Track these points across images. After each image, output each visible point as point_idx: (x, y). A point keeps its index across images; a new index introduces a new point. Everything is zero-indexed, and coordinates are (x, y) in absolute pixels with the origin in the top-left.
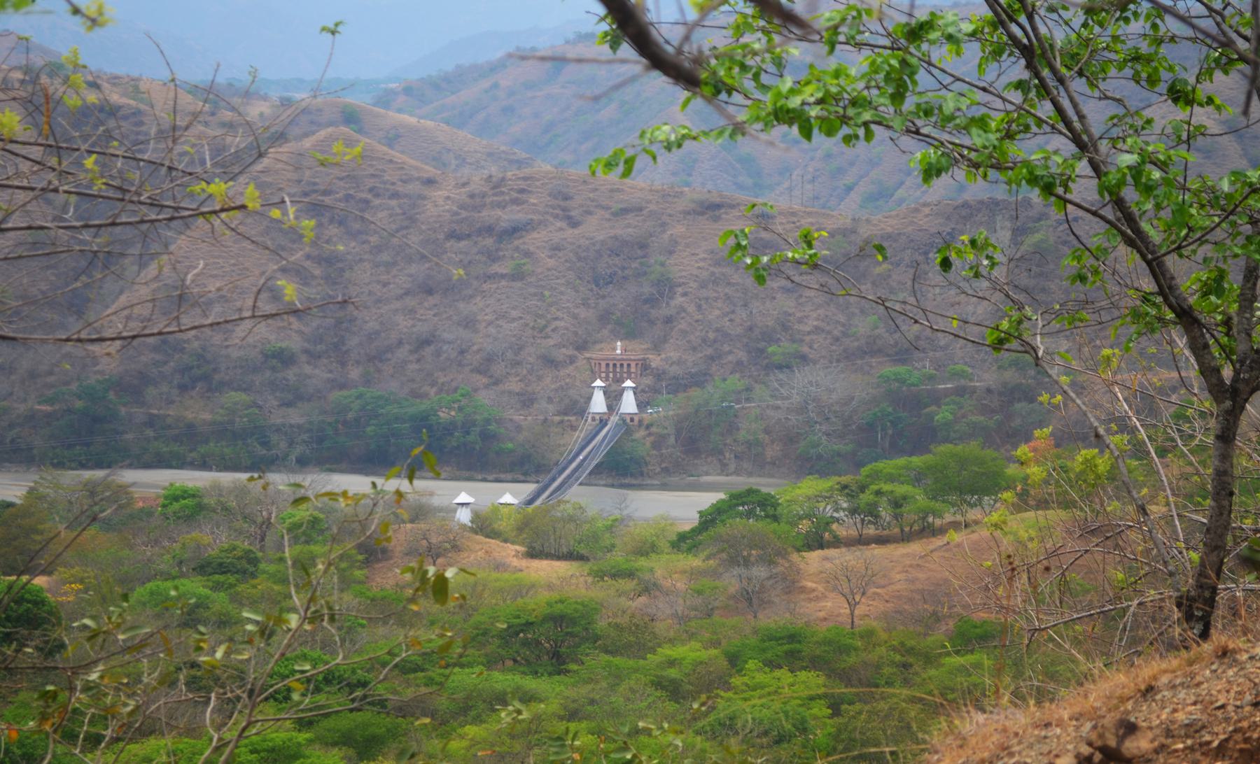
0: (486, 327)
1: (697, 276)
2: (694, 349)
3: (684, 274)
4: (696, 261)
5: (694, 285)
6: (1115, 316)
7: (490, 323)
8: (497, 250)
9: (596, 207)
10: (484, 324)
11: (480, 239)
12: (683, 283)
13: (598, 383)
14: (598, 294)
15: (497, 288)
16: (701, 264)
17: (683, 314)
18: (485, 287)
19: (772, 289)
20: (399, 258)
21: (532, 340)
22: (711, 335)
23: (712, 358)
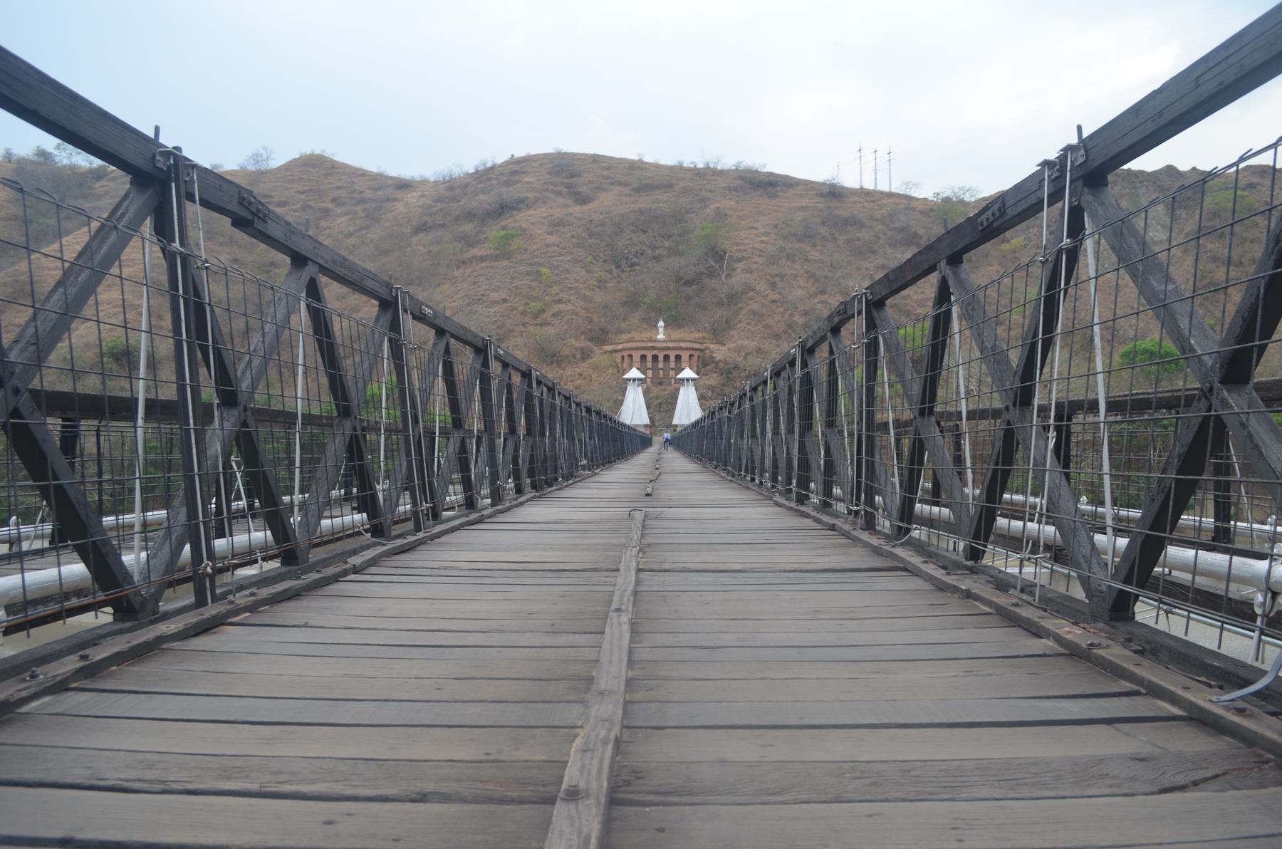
1: (761, 251)
2: (778, 337)
4: (757, 236)
5: (761, 260)
18: (457, 273)
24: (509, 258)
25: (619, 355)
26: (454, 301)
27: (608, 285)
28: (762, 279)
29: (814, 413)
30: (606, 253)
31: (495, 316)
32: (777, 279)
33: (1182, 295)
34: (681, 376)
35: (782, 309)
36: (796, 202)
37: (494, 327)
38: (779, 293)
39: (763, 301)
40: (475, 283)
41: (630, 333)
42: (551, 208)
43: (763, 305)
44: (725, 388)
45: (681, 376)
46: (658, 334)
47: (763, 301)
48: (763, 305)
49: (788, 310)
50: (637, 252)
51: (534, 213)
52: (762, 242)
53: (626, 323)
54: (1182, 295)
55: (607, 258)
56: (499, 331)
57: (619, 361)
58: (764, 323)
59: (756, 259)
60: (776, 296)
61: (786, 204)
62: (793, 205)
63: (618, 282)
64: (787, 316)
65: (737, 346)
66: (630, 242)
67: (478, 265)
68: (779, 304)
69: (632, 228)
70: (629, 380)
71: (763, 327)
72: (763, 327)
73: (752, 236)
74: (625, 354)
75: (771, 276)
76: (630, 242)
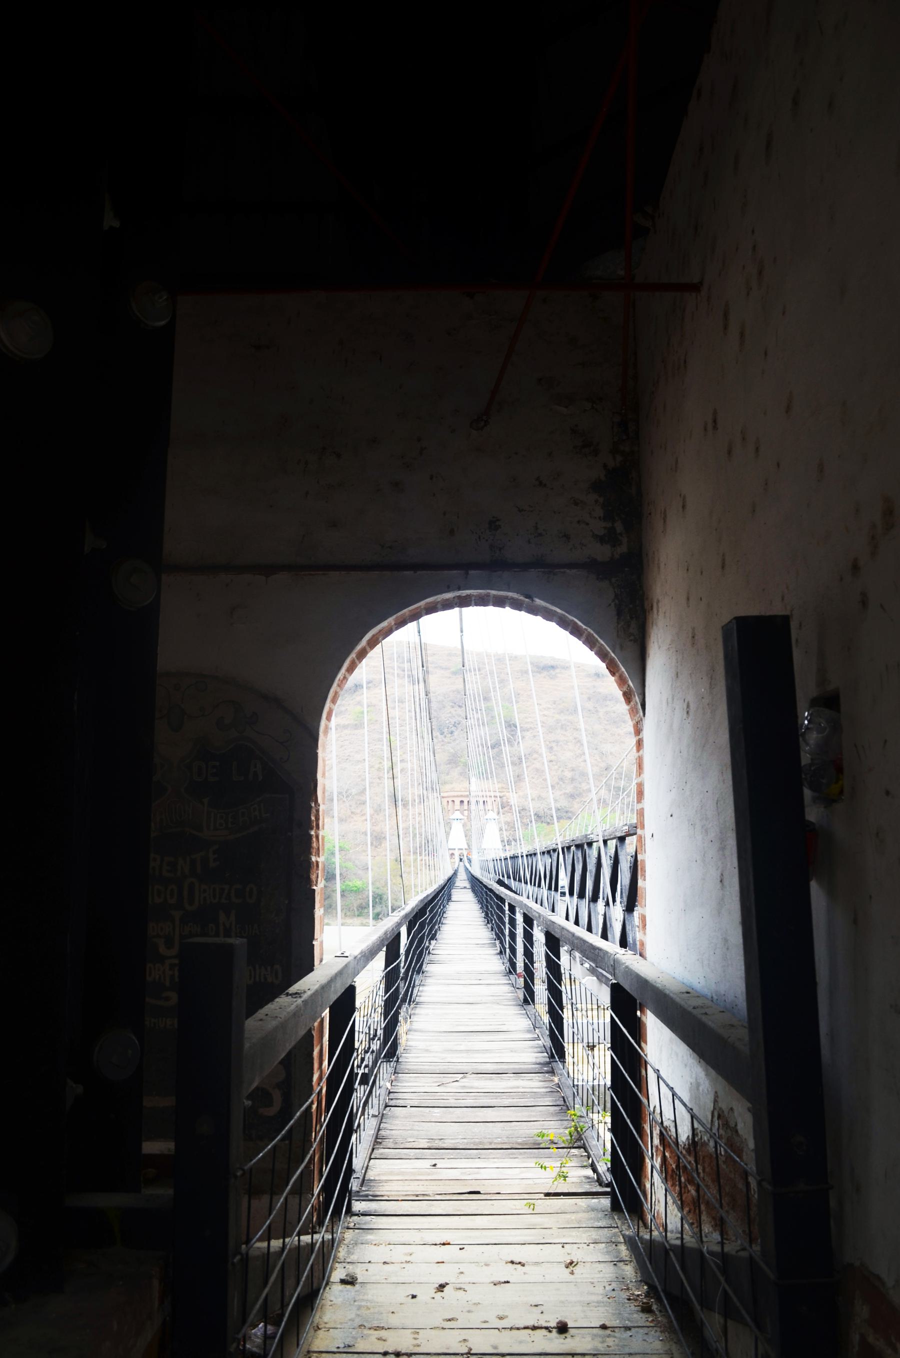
3: (529, 720)
9: (436, 667)
12: (531, 728)
13: (458, 815)
14: (443, 741)
16: (546, 712)
17: (535, 756)
19: (619, 735)
20: (579, 1109)
21: (378, 781)
22: (569, 775)
23: (572, 796)
25: (445, 800)
32: (554, 745)
38: (555, 755)
40: (342, 746)
50: (455, 723)
53: (449, 776)
57: (445, 803)
60: (553, 758)
66: (450, 715)
68: (554, 763)
69: (451, 704)
74: (450, 800)
75: (550, 742)
76: (450, 715)
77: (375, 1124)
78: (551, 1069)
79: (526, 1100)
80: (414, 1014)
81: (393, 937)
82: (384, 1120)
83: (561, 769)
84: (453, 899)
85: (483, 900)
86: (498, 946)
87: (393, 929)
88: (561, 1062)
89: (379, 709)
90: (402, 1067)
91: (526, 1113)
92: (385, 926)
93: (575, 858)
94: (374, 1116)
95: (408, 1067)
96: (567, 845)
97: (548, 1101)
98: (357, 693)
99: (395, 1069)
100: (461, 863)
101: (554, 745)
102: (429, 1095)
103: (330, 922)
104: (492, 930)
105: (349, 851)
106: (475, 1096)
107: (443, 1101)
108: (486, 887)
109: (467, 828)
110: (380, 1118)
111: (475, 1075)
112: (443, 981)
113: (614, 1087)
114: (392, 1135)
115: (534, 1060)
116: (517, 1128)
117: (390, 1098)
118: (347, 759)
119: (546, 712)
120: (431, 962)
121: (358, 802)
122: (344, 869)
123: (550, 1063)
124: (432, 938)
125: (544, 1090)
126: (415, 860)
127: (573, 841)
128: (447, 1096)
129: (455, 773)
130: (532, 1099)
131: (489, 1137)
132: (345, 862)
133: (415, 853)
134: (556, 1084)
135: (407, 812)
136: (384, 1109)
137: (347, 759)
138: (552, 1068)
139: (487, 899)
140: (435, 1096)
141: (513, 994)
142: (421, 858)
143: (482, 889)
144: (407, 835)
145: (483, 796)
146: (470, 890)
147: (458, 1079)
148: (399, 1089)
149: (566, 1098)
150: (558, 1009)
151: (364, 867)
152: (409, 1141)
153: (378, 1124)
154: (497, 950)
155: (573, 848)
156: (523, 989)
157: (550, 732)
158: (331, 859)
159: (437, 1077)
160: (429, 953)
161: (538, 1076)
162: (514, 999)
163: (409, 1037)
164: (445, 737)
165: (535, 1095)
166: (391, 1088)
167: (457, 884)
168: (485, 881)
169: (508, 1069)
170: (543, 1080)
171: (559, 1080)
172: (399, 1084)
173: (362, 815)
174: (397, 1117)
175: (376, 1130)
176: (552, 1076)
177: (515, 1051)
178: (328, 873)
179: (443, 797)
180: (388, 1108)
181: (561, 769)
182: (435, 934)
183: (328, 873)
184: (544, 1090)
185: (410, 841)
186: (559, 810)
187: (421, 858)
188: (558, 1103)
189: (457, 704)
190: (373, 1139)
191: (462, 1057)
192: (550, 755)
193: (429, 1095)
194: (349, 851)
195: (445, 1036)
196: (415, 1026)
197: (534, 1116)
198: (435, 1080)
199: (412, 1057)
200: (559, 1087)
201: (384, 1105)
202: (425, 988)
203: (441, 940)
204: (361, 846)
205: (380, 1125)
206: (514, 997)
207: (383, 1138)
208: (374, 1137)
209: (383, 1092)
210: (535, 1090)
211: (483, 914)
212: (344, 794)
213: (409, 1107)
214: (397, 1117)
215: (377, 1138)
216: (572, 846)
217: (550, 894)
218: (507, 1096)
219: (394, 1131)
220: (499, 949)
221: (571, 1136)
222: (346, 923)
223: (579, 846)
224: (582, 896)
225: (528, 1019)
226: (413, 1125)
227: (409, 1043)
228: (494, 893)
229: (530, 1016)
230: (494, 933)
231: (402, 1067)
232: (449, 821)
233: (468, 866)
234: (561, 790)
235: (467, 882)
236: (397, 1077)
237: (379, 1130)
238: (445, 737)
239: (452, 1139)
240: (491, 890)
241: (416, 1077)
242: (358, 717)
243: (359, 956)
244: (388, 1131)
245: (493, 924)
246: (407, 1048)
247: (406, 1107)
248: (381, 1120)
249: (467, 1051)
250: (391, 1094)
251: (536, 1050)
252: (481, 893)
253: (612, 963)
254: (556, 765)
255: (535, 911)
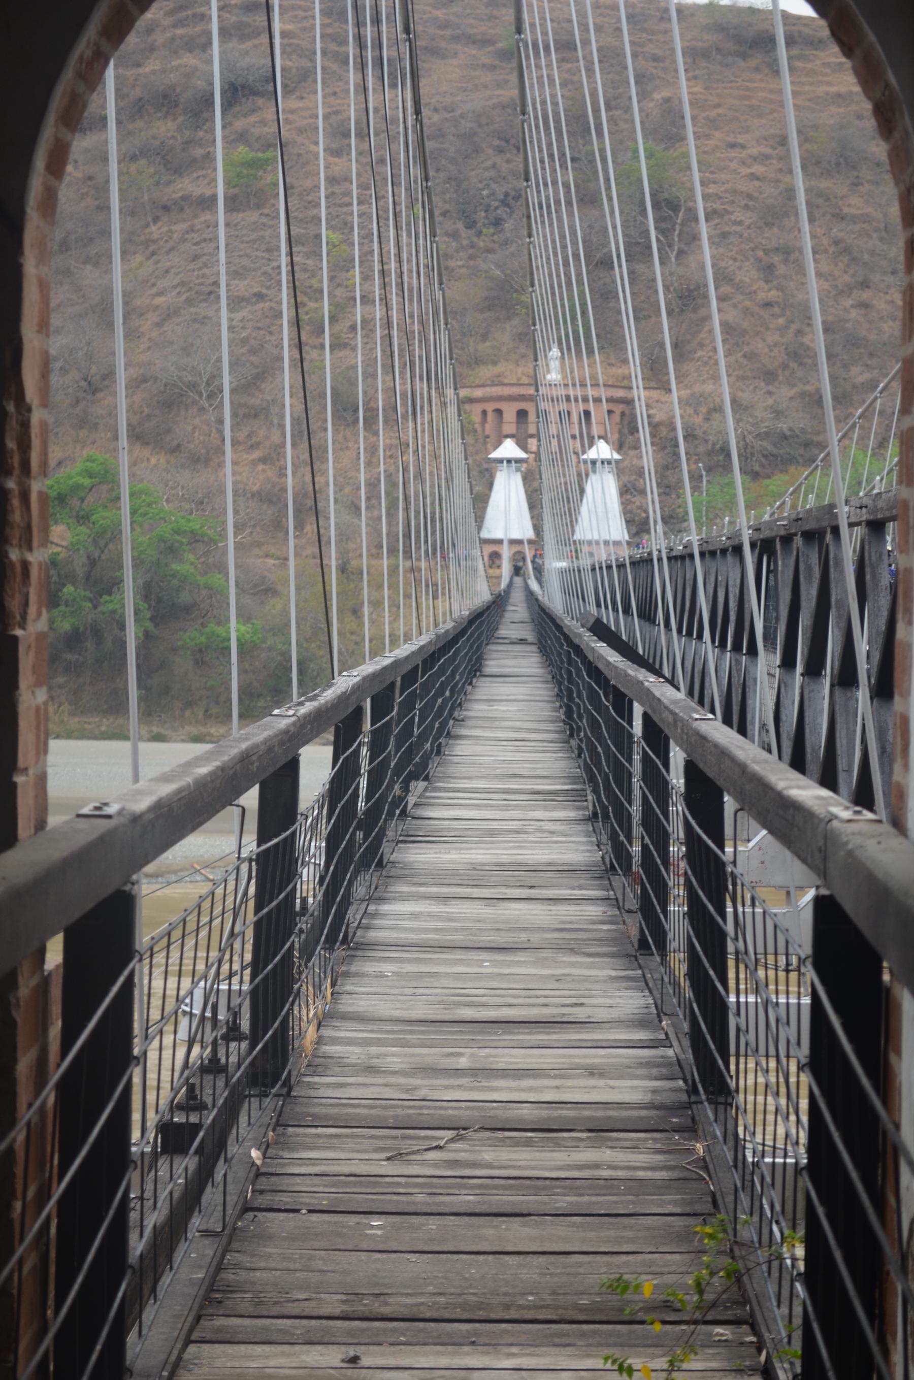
0: (158, 325)
1: (750, 196)
2: (770, 376)
4: (743, 163)
5: (747, 218)
6: (163, 961)
7: (169, 314)
8: (188, 143)
10: (153, 317)
11: (140, 124)
13: (509, 449)
14: (472, 246)
15: (191, 230)
16: (758, 169)
18: (155, 230)
24: (258, 206)
25: (477, 409)
26: (160, 294)
27: (452, 264)
28: (747, 259)
29: (808, 642)
30: (448, 196)
31: (243, 328)
32: (776, 259)
33: (299, 1120)
34: (592, 454)
35: (781, 321)
36: (828, 83)
37: (244, 350)
38: (780, 288)
39: (747, 303)
40: (195, 258)
41: (495, 363)
42: (335, 93)
43: (746, 311)
44: (669, 473)
45: (592, 454)
46: (548, 372)
47: (747, 303)
48: (746, 311)
49: (792, 322)
50: (506, 195)
51: (300, 104)
52: (754, 177)
53: (488, 344)
54: (299, 1120)
55: (447, 207)
56: (254, 359)
57: (476, 418)
58: (746, 349)
59: (738, 215)
60: (773, 295)
61: (807, 88)
62: (821, 90)
63: (472, 257)
64: (790, 335)
65: (692, 395)
66: (492, 173)
67: (196, 216)
68: (776, 310)
69: (497, 142)
70: (501, 461)
71: (745, 356)
72: (745, 356)
73: (733, 165)
74: (490, 407)
75: (766, 252)
76: (492, 173)
77: (211, 1253)
78: (689, 1122)
79: (614, 1198)
80: (347, 975)
81: (271, 770)
82: (235, 1245)
83: (794, 327)
84: (487, 670)
85: (562, 676)
86: (590, 798)
87: (270, 750)
88: (710, 1103)
89: (299, 155)
90: (298, 1109)
91: (611, 1233)
92: (246, 739)
93: (802, 567)
94: (207, 1233)
95: (316, 1110)
96: (782, 532)
97: (670, 1202)
98: (238, 108)
99: (280, 1116)
100: (518, 580)
101: (776, 259)
102: (360, 1183)
103: (163, 731)
104: (579, 756)
105: (216, 542)
106: (480, 1186)
107: (395, 1197)
108: (568, 639)
109: (535, 484)
110: (225, 1239)
111: (488, 1134)
112: (434, 890)
113: (814, 1168)
114: (253, 1283)
115: (648, 1098)
116: (581, 1270)
117: (258, 1187)
118: (210, 293)
119: (758, 169)
120: (409, 838)
121: (241, 412)
122: (204, 592)
123: (689, 1105)
124: (414, 776)
125: (663, 1175)
126: (394, 570)
127: (797, 520)
128: (407, 1185)
129: (504, 335)
130: (630, 1198)
131: (504, 1290)
132: (205, 573)
133: (393, 551)
134: (699, 1159)
135: (375, 439)
136: (240, 1217)
137: (210, 293)
138: (693, 1119)
139: (569, 673)
140: (375, 1184)
141: (613, 927)
142: (408, 564)
143: (561, 646)
144: (374, 501)
145: (585, 400)
146: (534, 648)
147: (442, 1143)
148: (283, 1165)
149: (718, 1197)
150: (707, 965)
151: (256, 586)
152: (295, 1297)
153: (218, 1254)
154: (587, 808)
155: (798, 541)
156: (639, 914)
157: (766, 224)
158: (166, 565)
159: (387, 1137)
160: (404, 813)
161: (653, 1139)
162: (614, 939)
163: (326, 1032)
164: (479, 233)
165: (638, 1186)
166: (263, 1164)
167: (503, 632)
168: (568, 622)
169: (579, 1119)
170: (665, 1148)
171: (708, 1149)
172: (287, 1155)
173: (252, 446)
174: (270, 1237)
175: (212, 1269)
176: (689, 1140)
177: (601, 1075)
178: (159, 600)
179: (471, 400)
180: (250, 1215)
181: (794, 327)
182: (424, 764)
183: (159, 600)
184: (663, 1175)
185: (380, 518)
186: (786, 437)
187: (408, 564)
188: (698, 1208)
189: (513, 141)
190: (202, 1292)
191: (459, 1086)
192: (766, 287)
193: (360, 1183)
194: (216, 542)
195: (423, 1032)
196: (347, 1005)
197: (631, 1241)
198: (380, 1144)
199: (328, 1085)
200: (706, 1168)
201: (239, 1207)
202: (386, 908)
203: (440, 779)
204: (248, 531)
205: (223, 1256)
206: (615, 935)
207: (229, 1289)
208: (204, 1288)
209: (238, 1172)
210: (641, 1174)
211: (562, 711)
212: (202, 387)
213: (304, 1211)
214: (270, 1237)
215: (211, 1289)
216: (796, 535)
217: (738, 663)
218: (564, 1188)
219: (258, 1274)
220: (591, 808)
221: (701, 1292)
222: (209, 734)
223: (811, 536)
224: (814, 669)
225: (647, 993)
226: (311, 1258)
227: (328, 1049)
228: (584, 658)
229: (651, 985)
230: (581, 762)
231: (298, 1109)
232: (485, 466)
233: (534, 585)
234: (794, 385)
235: (529, 627)
236: (284, 1134)
237: (220, 1268)
238: (479, 233)
239: (408, 1294)
240: (578, 650)
241: (331, 1136)
242: (239, 175)
243: (151, 816)
244: (243, 1273)
245: (581, 740)
246: (317, 1061)
247: (297, 1211)
248: (229, 1243)
249: (474, 1072)
250: (263, 1179)
251: (655, 1071)
252: (559, 654)
253: (821, 843)
254: (783, 315)
255: (666, 708)
